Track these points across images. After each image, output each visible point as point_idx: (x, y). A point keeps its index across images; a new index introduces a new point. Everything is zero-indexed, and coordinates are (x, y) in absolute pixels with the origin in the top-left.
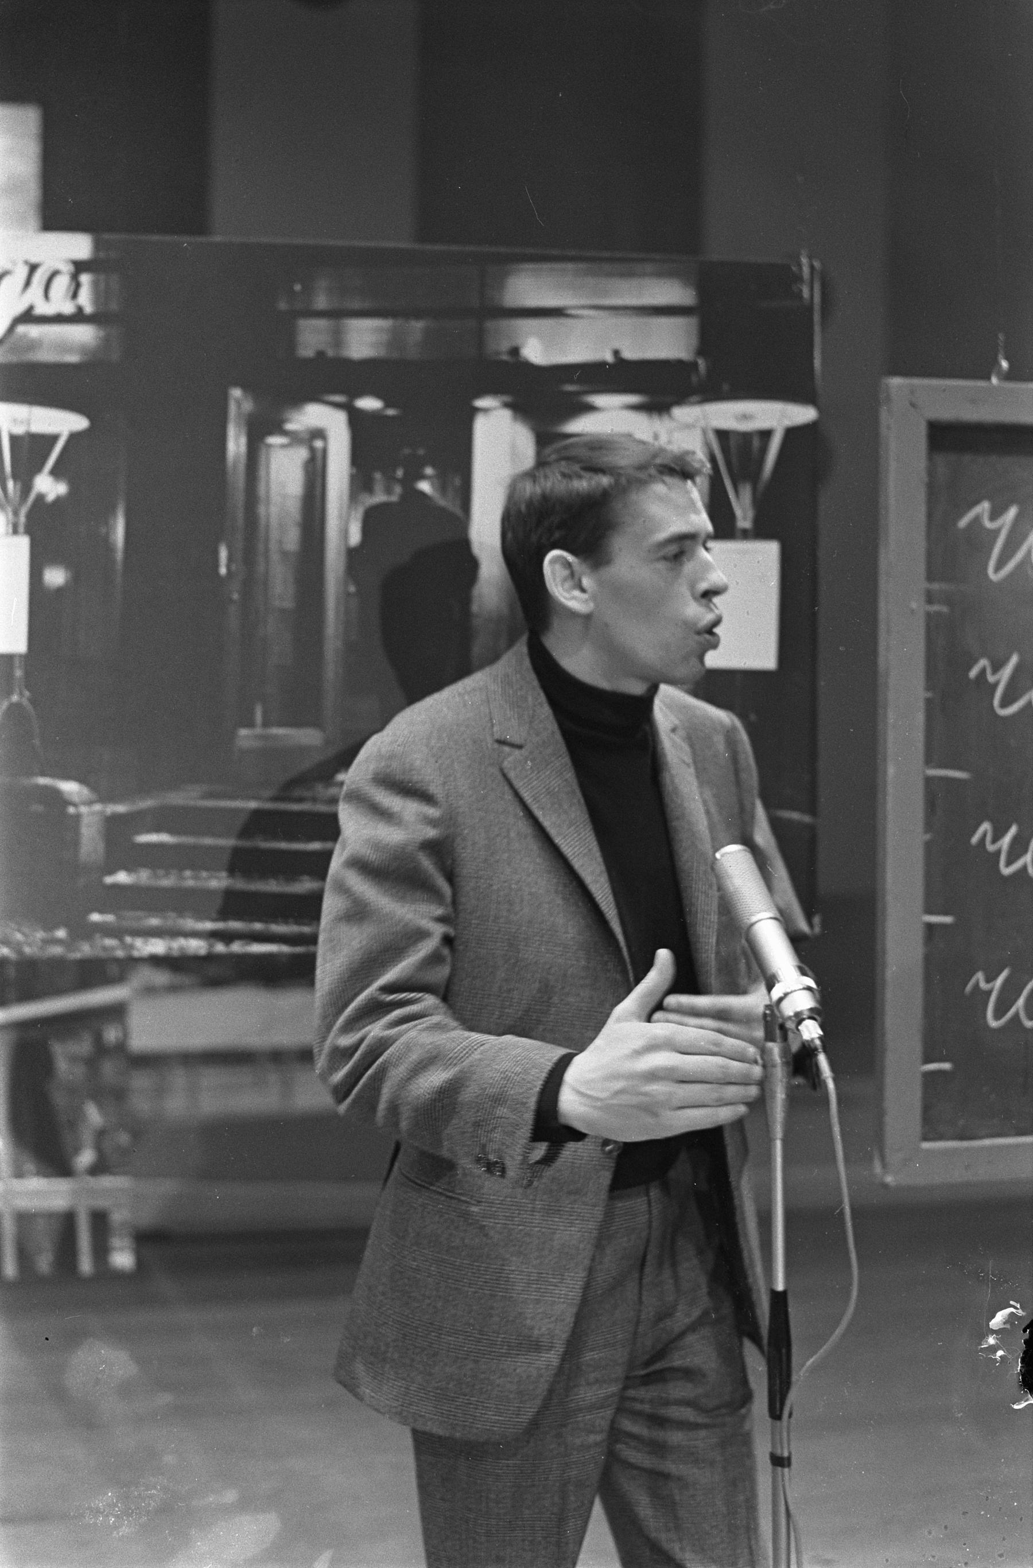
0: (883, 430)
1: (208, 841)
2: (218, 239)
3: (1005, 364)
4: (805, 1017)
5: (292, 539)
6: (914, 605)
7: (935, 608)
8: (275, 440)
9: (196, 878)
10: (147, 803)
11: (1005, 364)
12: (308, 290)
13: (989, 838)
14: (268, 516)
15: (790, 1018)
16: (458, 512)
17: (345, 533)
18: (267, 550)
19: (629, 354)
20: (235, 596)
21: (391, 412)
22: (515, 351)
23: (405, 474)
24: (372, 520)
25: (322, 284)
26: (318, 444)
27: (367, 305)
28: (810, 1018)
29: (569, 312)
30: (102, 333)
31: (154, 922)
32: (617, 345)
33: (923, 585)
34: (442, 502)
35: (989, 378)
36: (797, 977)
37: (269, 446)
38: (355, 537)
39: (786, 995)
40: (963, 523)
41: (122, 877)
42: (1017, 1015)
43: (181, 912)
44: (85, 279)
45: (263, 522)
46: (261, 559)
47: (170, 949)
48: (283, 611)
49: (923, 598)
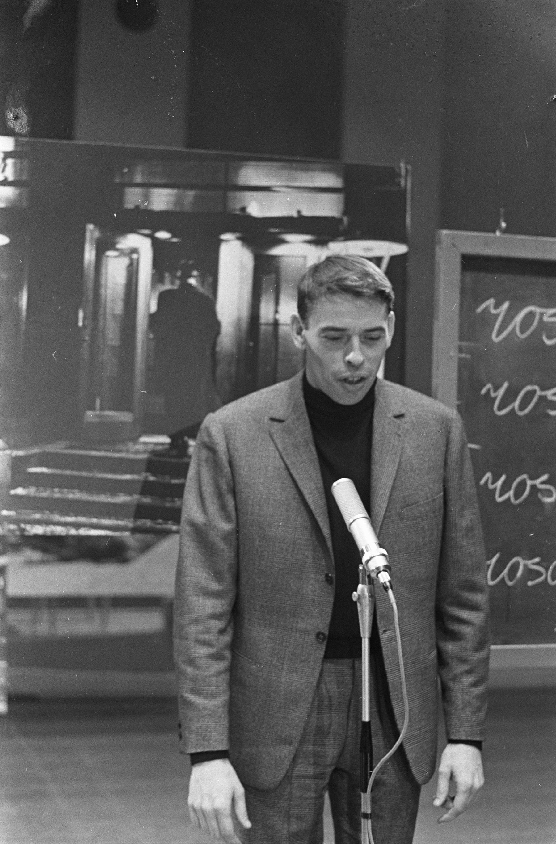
0: (437, 259)
1: (68, 472)
2: (82, 142)
3: (504, 225)
4: (381, 570)
5: (119, 308)
6: (452, 353)
7: (463, 355)
8: (110, 253)
9: (61, 492)
10: (34, 451)
11: (504, 225)
12: (132, 172)
13: (490, 482)
14: (106, 296)
15: (373, 571)
16: (211, 296)
17: (148, 306)
18: (105, 314)
19: (306, 213)
20: (87, 338)
21: (175, 240)
22: (244, 209)
23: (182, 274)
24: (163, 298)
25: (139, 168)
26: (135, 256)
27: (163, 181)
28: (384, 571)
29: (274, 189)
30: (18, 192)
31: (37, 516)
32: (299, 208)
33: (457, 343)
34: (201, 290)
35: (494, 232)
36: (377, 548)
37: (108, 256)
38: (153, 308)
39: (371, 558)
40: (479, 310)
41: (20, 491)
42: (503, 579)
43: (52, 512)
44: (10, 161)
45: (103, 297)
46: (101, 318)
47: (45, 531)
48: (113, 347)
49: (456, 350)
